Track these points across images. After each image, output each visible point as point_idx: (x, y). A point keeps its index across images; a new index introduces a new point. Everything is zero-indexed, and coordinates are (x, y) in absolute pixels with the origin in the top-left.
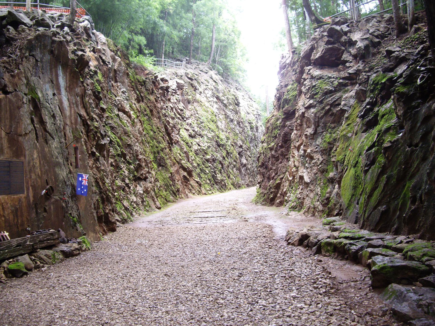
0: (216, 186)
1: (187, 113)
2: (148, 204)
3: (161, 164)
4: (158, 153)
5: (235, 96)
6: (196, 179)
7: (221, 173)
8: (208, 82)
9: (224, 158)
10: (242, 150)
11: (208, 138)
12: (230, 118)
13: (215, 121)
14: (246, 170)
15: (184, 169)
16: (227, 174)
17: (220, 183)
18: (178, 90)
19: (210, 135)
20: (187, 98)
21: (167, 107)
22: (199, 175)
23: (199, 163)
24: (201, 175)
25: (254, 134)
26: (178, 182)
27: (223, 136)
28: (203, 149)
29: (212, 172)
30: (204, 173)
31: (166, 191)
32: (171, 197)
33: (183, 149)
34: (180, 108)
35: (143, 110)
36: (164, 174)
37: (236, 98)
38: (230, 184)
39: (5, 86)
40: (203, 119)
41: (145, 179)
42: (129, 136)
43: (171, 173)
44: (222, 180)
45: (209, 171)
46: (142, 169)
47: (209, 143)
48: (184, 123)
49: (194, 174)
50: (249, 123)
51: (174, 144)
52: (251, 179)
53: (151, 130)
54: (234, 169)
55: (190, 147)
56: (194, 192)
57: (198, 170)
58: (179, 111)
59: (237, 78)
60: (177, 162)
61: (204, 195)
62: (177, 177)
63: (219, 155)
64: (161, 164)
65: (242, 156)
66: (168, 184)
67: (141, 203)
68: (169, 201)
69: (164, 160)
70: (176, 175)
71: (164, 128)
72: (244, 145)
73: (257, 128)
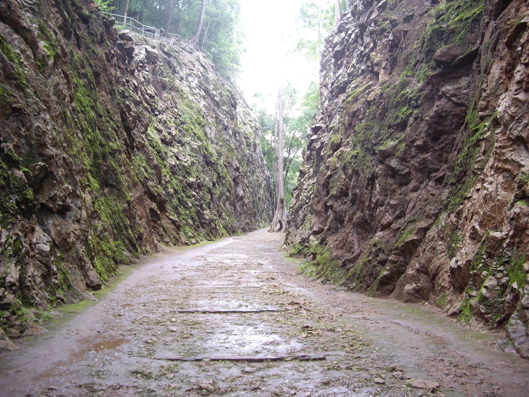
0: (203, 230)
1: (161, 105)
2: (66, 279)
3: (109, 182)
4: (104, 157)
5: (230, 92)
6: (171, 217)
7: (209, 208)
8: (194, 66)
9: (214, 184)
10: (238, 174)
11: (192, 149)
12: (224, 125)
13: (203, 124)
14: (243, 206)
15: (152, 197)
16: (218, 211)
17: (209, 225)
18: (148, 64)
19: (195, 145)
20: (162, 80)
21: (128, 81)
22: (176, 209)
23: (177, 188)
24: (180, 209)
25: (251, 155)
26: (140, 220)
27: (212, 149)
28: (184, 166)
29: (197, 205)
30: (185, 207)
31: (115, 239)
32: (126, 253)
33: (152, 160)
34: (149, 92)
35: (78, 64)
36: (113, 204)
37: (232, 95)
38: (221, 226)
39: (6, 142)
40: (185, 117)
41: (63, 211)
42: (20, 88)
43: (128, 202)
44: (212, 221)
45: (192, 204)
46: (53, 186)
47: (193, 157)
48: (154, 118)
49: (168, 207)
50: (245, 137)
51: (135, 150)
52: (247, 220)
53: (93, 108)
54: (227, 204)
55: (163, 160)
56: (167, 239)
57: (175, 201)
58: (148, 97)
59: (229, 73)
60: (140, 181)
61: (185, 247)
62: (139, 211)
63: (207, 179)
64: (109, 182)
65: (238, 183)
66: (121, 224)
67: (39, 280)
68: (122, 262)
69: (116, 174)
70: (137, 207)
71: (119, 115)
72: (241, 168)
73: (255, 145)
